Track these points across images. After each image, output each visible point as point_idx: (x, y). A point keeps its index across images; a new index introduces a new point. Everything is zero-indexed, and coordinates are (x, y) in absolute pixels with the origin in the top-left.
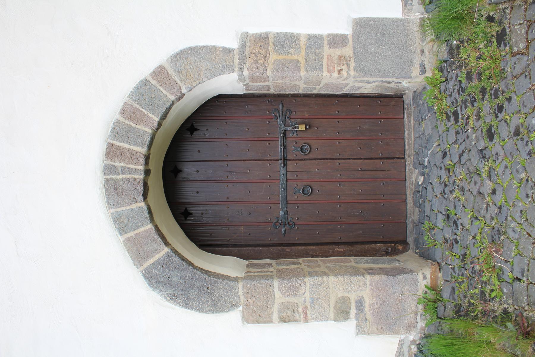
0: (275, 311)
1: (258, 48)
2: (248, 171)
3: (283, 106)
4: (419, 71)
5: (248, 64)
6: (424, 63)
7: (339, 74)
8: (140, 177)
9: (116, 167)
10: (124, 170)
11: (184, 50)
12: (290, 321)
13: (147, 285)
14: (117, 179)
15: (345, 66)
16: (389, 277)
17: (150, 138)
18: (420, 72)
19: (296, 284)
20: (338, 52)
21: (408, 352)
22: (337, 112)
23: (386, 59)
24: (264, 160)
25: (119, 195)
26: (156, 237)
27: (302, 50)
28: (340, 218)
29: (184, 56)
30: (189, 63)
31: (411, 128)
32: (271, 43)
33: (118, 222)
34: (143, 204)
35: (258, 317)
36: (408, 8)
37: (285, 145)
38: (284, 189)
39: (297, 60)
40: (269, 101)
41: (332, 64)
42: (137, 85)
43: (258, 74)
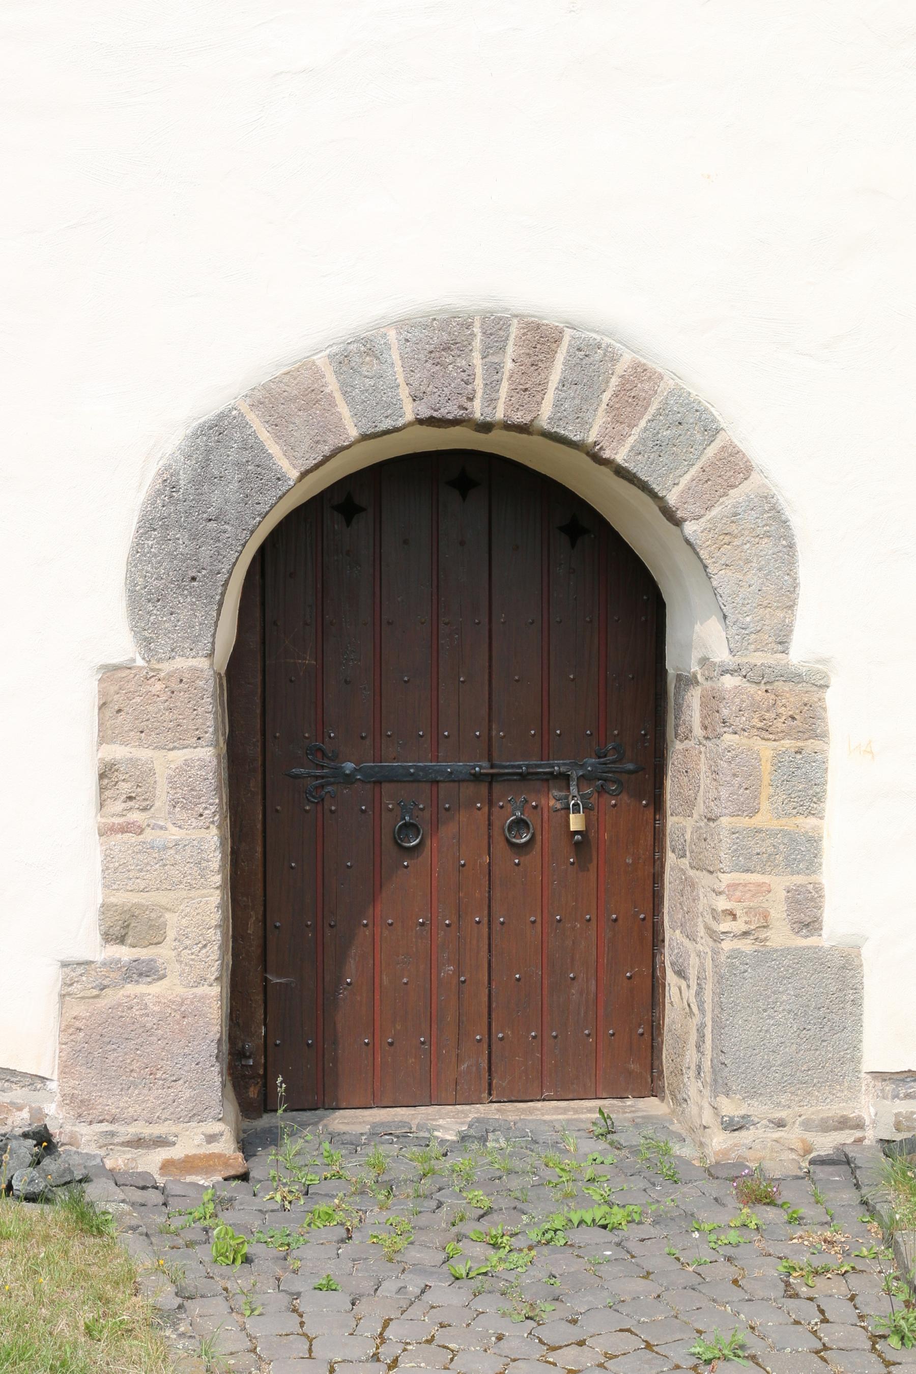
0: (131, 750)
1: (791, 713)
2: (462, 679)
3: (630, 772)
4: (732, 1114)
5: (752, 689)
6: (751, 1127)
7: (723, 911)
8: (478, 410)
9: (503, 349)
10: (497, 369)
11: (788, 528)
12: (102, 789)
13: (201, 421)
14: (471, 350)
15: (744, 928)
16: (214, 1045)
17: (575, 439)
18: (729, 1117)
19: (204, 805)
20: (778, 912)
21: (12, 1104)
22: (614, 916)
23: (760, 1031)
24: (490, 721)
25: (433, 355)
26: (327, 449)
27: (784, 821)
28: (331, 926)
29: (773, 528)
30: (757, 540)
31: (574, 1114)
32: (800, 744)
33: (363, 349)
34: (409, 417)
35: (116, 708)
36: (888, 1088)
37: (530, 777)
38: (412, 774)
39: (759, 809)
40: (645, 735)
41: (748, 895)
42: (706, 409)
43: (725, 712)
